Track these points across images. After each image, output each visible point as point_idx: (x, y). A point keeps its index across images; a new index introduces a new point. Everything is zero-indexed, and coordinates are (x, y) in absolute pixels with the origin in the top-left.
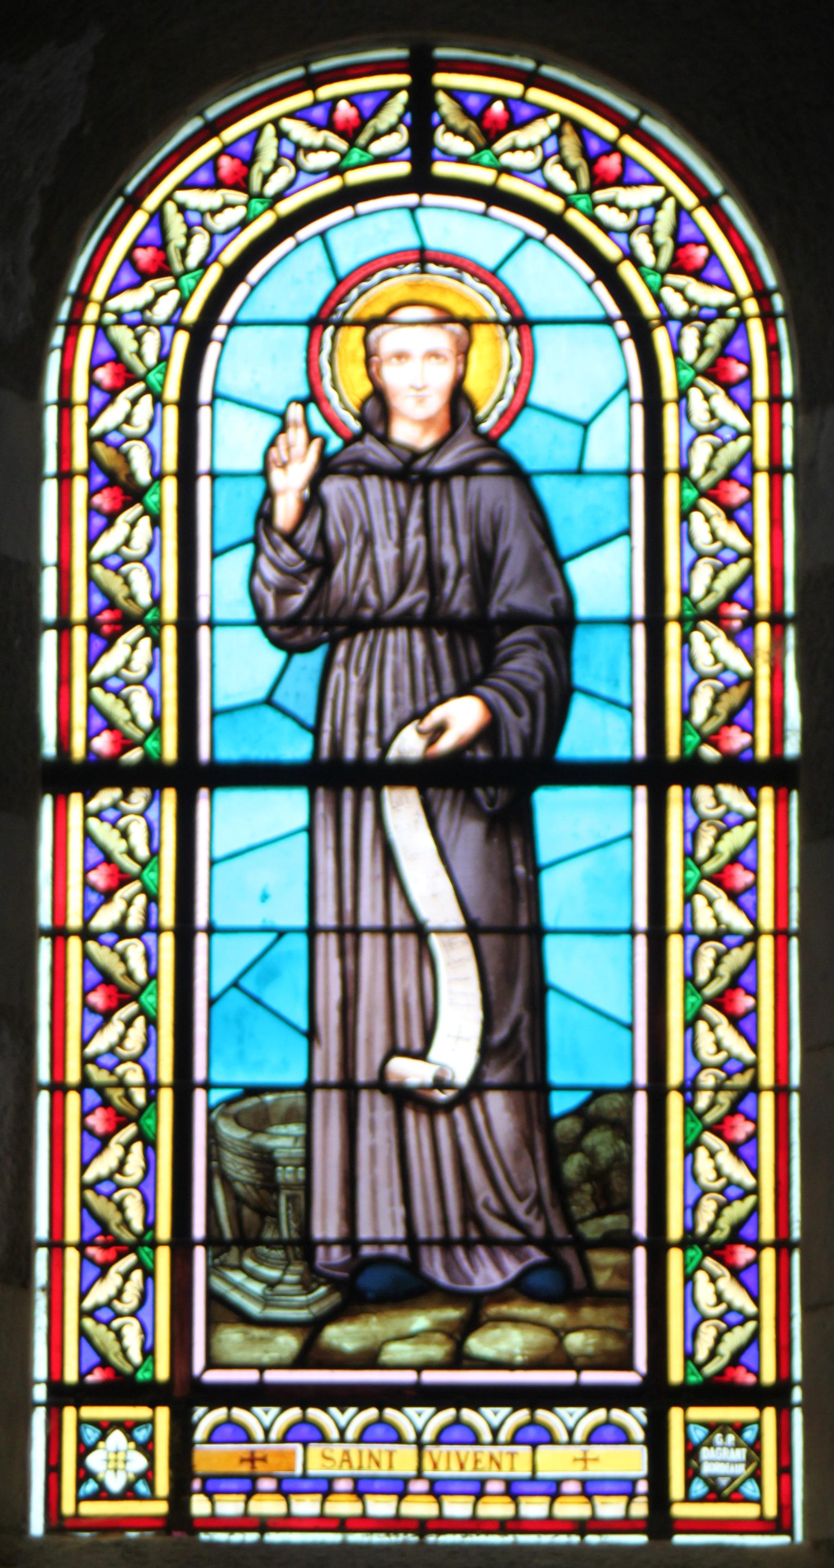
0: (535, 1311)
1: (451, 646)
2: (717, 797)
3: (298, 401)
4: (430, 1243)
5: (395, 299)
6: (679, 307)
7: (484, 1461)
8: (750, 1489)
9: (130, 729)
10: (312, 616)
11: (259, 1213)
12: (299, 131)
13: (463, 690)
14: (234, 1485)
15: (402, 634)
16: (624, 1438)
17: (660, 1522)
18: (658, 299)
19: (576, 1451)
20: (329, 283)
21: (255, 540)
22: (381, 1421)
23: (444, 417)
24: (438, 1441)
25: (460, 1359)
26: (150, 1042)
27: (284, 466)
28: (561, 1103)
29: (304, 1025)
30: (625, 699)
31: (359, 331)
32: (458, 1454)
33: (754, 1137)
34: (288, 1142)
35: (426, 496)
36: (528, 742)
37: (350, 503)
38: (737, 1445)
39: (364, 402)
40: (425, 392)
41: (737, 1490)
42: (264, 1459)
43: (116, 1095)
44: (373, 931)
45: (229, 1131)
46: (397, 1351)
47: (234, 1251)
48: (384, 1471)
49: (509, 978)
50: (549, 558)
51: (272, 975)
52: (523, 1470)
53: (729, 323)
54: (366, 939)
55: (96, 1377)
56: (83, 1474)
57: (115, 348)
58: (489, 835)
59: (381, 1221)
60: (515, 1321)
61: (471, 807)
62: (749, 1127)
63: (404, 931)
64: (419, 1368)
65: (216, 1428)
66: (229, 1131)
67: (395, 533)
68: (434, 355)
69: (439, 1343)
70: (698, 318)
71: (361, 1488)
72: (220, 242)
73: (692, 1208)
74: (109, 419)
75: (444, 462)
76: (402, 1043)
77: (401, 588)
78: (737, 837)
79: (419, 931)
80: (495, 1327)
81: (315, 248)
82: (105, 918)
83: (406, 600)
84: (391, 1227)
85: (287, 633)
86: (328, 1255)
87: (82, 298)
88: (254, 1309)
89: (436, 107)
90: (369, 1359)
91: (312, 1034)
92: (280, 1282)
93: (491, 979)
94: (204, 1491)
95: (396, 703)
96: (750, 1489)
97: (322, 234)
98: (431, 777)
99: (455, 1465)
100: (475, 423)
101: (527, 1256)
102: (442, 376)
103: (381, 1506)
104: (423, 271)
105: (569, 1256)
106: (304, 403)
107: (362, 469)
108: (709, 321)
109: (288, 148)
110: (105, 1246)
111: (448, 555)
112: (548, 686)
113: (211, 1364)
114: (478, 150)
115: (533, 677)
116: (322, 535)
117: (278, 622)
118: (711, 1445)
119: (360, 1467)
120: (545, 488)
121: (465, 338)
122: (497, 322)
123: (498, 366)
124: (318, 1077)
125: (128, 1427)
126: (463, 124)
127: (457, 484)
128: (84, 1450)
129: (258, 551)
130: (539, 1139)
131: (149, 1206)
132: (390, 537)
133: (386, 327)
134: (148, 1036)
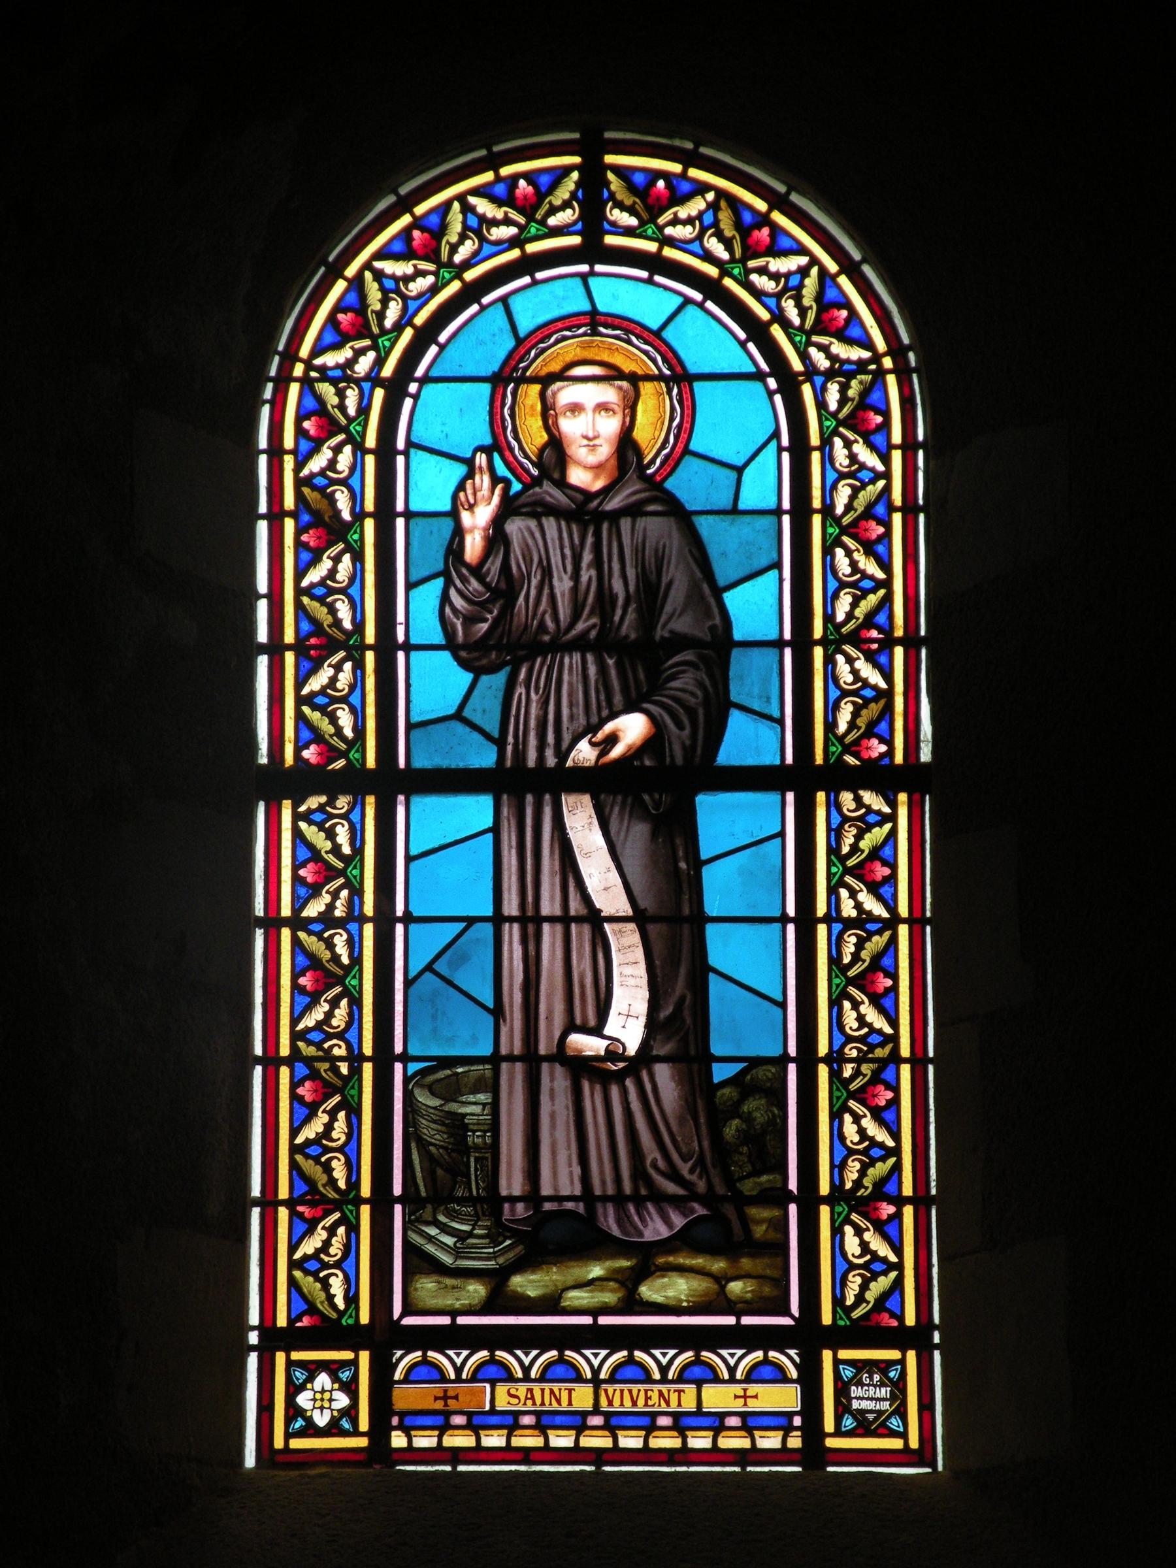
0: (699, 1261)
1: (619, 665)
2: (858, 800)
3: (481, 449)
4: (605, 1199)
5: (569, 358)
6: (822, 362)
7: (655, 1396)
8: (895, 1423)
9: (336, 741)
10: (494, 638)
11: (450, 1172)
12: (483, 206)
13: (629, 708)
14: (428, 1421)
15: (577, 657)
16: (781, 1377)
17: (814, 1452)
18: (804, 357)
19: (737, 1389)
20: (510, 343)
21: (445, 573)
22: (561, 1360)
23: (613, 462)
24: (612, 1380)
25: (633, 1304)
26: (354, 1018)
27: (471, 507)
28: (721, 1072)
29: (490, 1004)
30: (776, 714)
31: (536, 388)
32: (630, 1391)
33: (895, 1102)
34: (477, 1109)
35: (598, 535)
36: (689, 751)
37: (530, 542)
38: (882, 1384)
39: (542, 450)
40: (597, 442)
41: (883, 1424)
42: (456, 1398)
43: (323, 1067)
44: (551, 919)
45: (424, 1098)
46: (577, 1297)
47: (429, 1208)
48: (564, 1406)
49: (673, 961)
50: (709, 591)
51: (464, 959)
52: (689, 1404)
53: (868, 378)
54: (546, 927)
55: (305, 1322)
56: (293, 1411)
57: (320, 399)
58: (654, 835)
59: (560, 1177)
60: (682, 1270)
61: (638, 811)
62: (890, 1095)
63: (578, 919)
64: (595, 1312)
65: (412, 1367)
66: (424, 1098)
67: (569, 568)
68: (602, 407)
69: (612, 1291)
70: (840, 373)
71: (544, 1422)
72: (413, 305)
73: (838, 1168)
74: (317, 464)
75: (614, 503)
76: (578, 1021)
77: (576, 616)
78: (878, 834)
79: (595, 919)
80: (663, 1276)
81: (497, 315)
82: (313, 909)
83: (580, 626)
84: (569, 1185)
85: (472, 654)
86: (513, 1210)
87: (290, 356)
88: (447, 1259)
89: (607, 184)
90: (551, 1304)
91: (498, 1012)
92: (470, 1234)
93: (656, 953)
94: (400, 1427)
95: (572, 717)
96: (895, 1423)
97: (504, 300)
98: (609, 785)
99: (628, 1402)
100: (642, 468)
101: (693, 1211)
102: (610, 426)
103: (562, 1440)
104: (595, 333)
105: (729, 1211)
106: (487, 450)
107: (539, 510)
108: (850, 375)
109: (473, 221)
110: (311, 1204)
111: (617, 585)
112: (706, 702)
113: (406, 1312)
114: (643, 223)
115: (693, 694)
116: (505, 566)
117: (464, 647)
118: (860, 1384)
119: (543, 1404)
120: (704, 524)
121: (632, 393)
122: (660, 377)
123: (662, 418)
124: (504, 1051)
125: (332, 1368)
126: (628, 200)
127: (625, 524)
128: (293, 1390)
129: (449, 583)
130: (700, 1105)
131: (353, 1168)
132: (565, 572)
133: (559, 384)
134: (350, 1014)
